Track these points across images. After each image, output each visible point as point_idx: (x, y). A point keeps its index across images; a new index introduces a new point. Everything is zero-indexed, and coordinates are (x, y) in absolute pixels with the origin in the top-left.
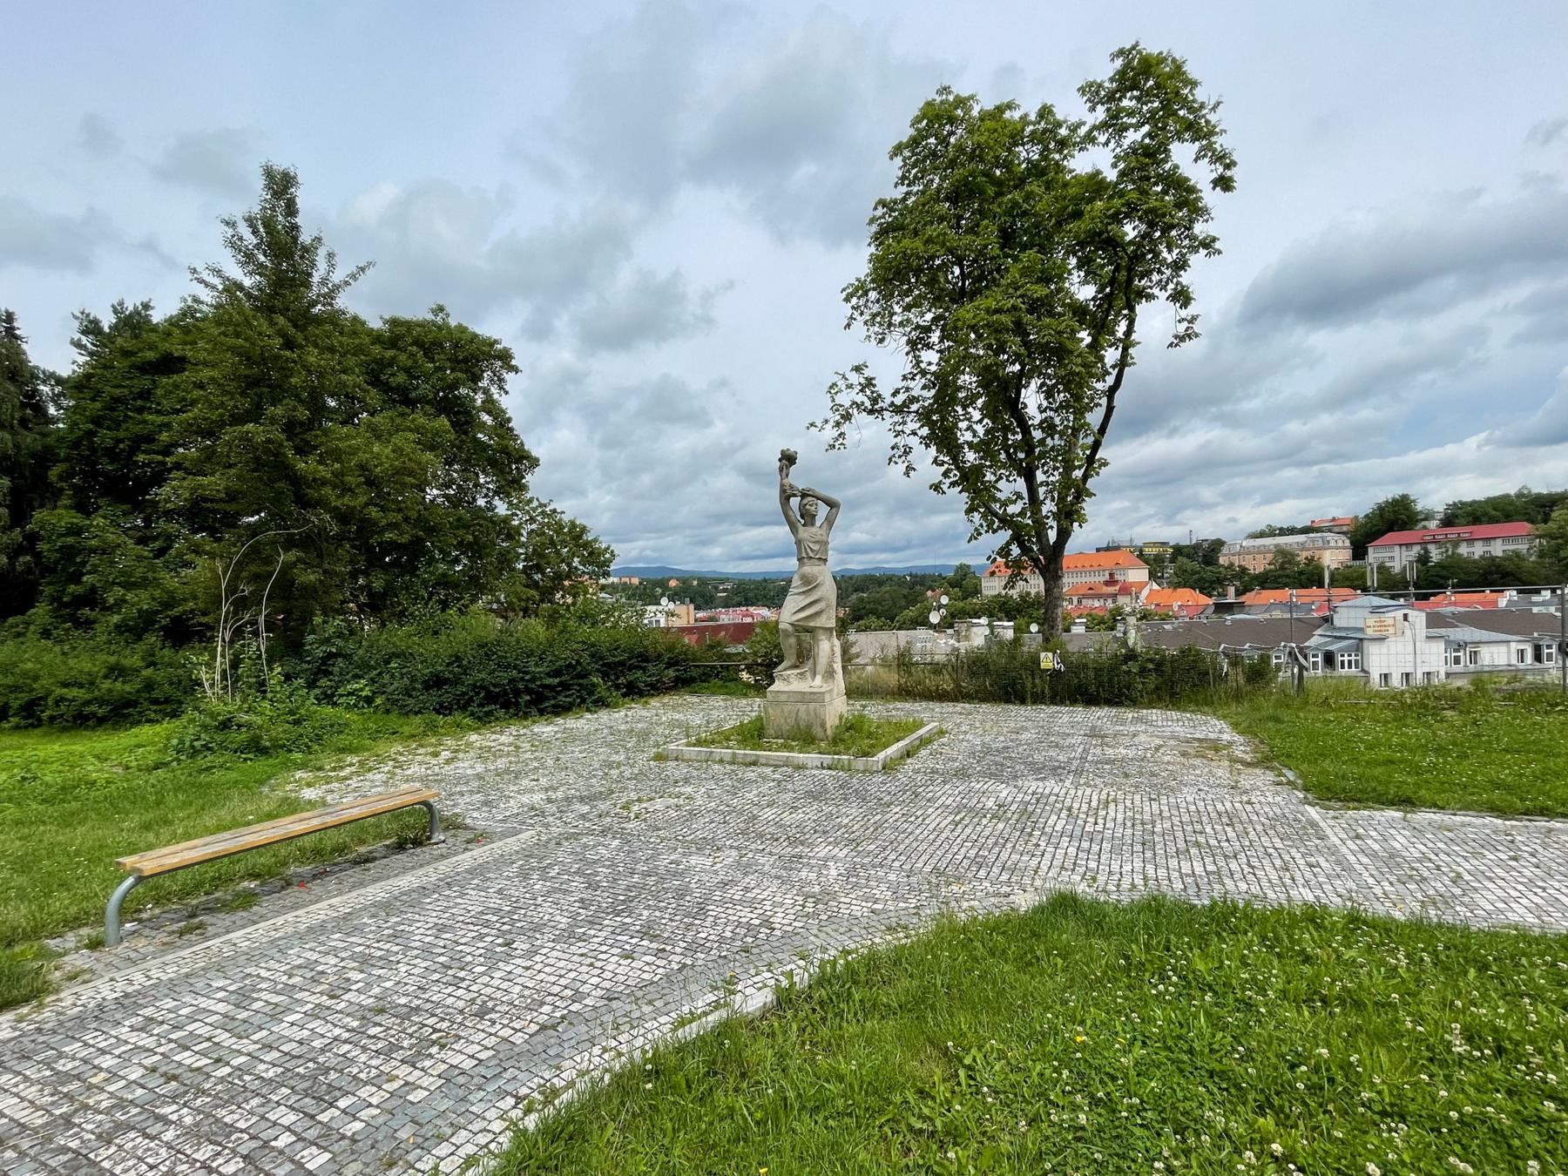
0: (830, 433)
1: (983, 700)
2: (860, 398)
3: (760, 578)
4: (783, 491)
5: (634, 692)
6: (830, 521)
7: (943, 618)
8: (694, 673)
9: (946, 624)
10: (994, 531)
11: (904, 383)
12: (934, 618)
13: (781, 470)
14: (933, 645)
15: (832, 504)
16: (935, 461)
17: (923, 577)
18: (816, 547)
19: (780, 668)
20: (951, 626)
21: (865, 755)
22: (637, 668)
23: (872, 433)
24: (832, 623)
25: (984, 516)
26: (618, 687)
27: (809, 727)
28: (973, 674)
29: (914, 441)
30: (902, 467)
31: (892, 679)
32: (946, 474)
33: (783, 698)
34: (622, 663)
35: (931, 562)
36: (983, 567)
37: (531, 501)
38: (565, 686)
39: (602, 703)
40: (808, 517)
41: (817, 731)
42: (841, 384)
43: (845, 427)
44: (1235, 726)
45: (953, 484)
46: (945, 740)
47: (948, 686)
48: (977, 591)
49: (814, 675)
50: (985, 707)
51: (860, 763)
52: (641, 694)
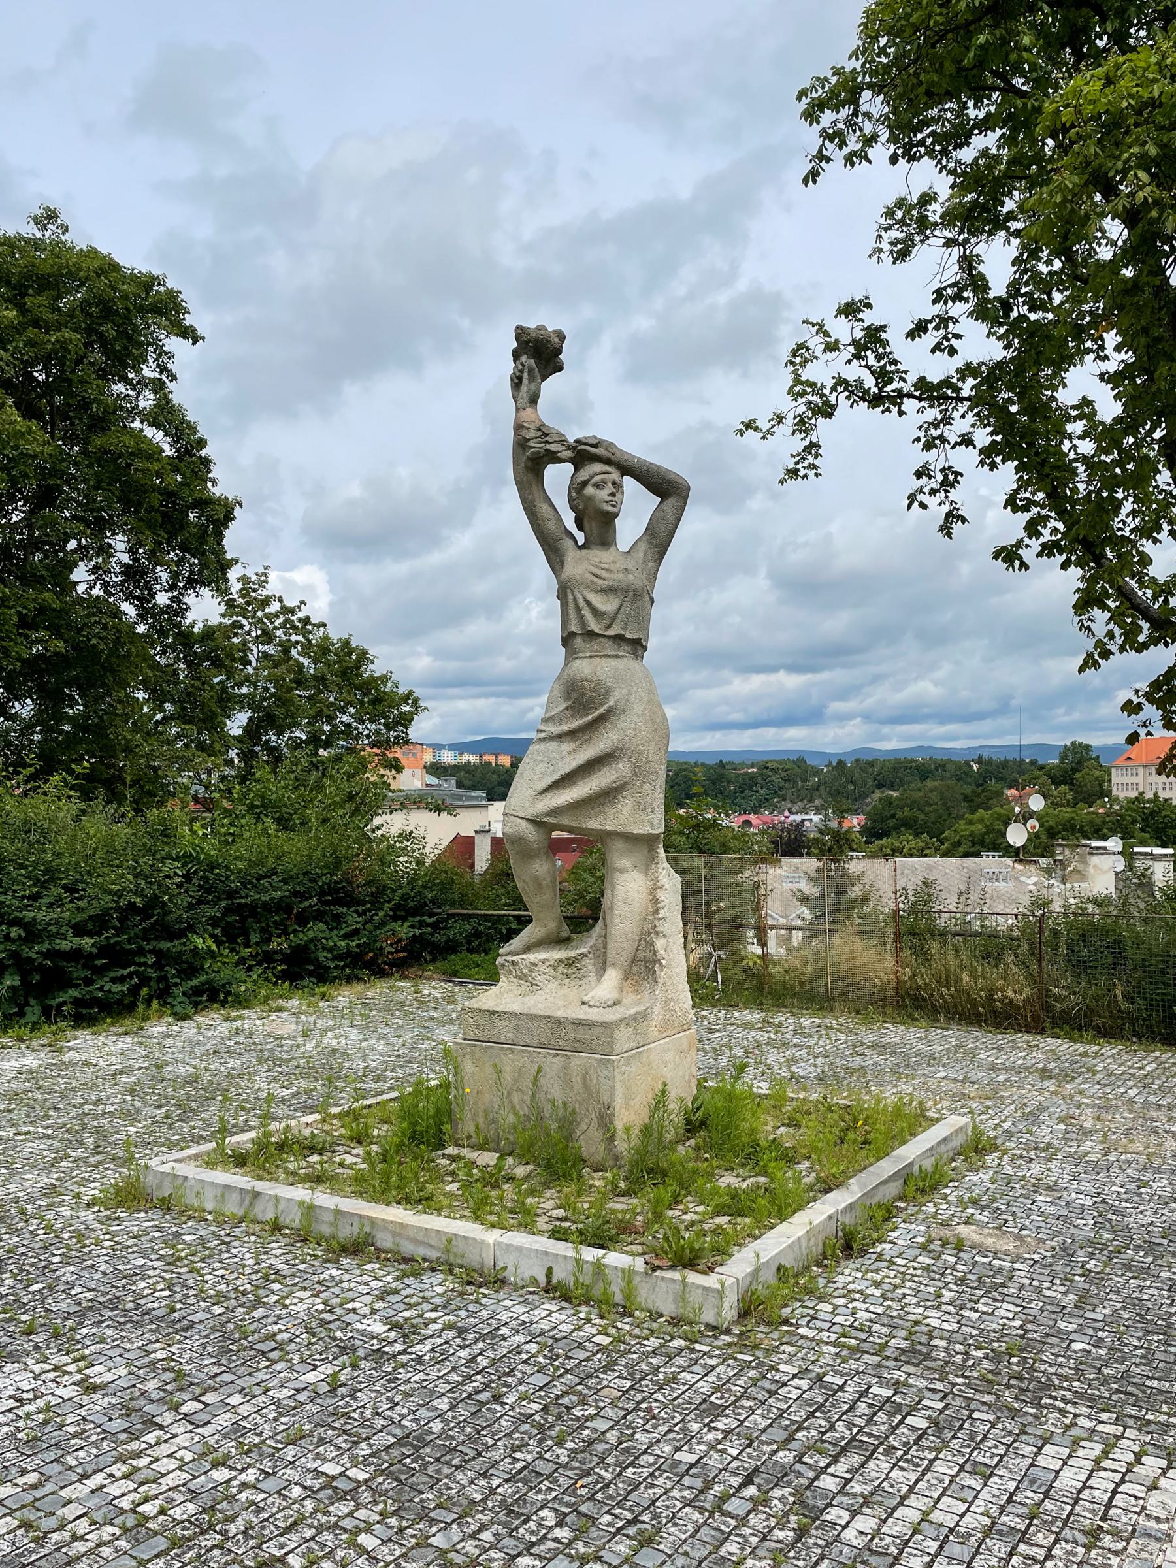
1: (1108, 1034)
2: (854, 372)
3: (712, 762)
4: (521, 444)
5: (303, 971)
6: (659, 538)
7: (1033, 838)
8: (457, 931)
9: (1038, 849)
10: (1144, 647)
11: (937, 309)
12: (1016, 836)
13: (517, 382)
14: (1000, 890)
15: (666, 488)
16: (1012, 503)
17: (1004, 764)
18: (608, 605)
19: (516, 943)
20: (1047, 851)
21: (688, 1260)
22: (319, 916)
23: (874, 447)
24: (654, 822)
25: (1116, 617)
26: (268, 958)
27: (568, 1125)
28: (1080, 966)
29: (965, 459)
30: (937, 510)
31: (880, 964)
32: (1032, 529)
33: (505, 1031)
34: (283, 907)
35: (1012, 740)
36: (1114, 750)
37: (266, 601)
38: (115, 956)
39: (214, 996)
40: (598, 523)
41: (589, 1142)
42: (816, 343)
43: (823, 428)
44: (331, 583)
45: (1048, 549)
46: (980, 1179)
47: (1015, 989)
48: (1101, 790)
50: (1110, 1056)
51: (663, 1291)
52: (323, 976)
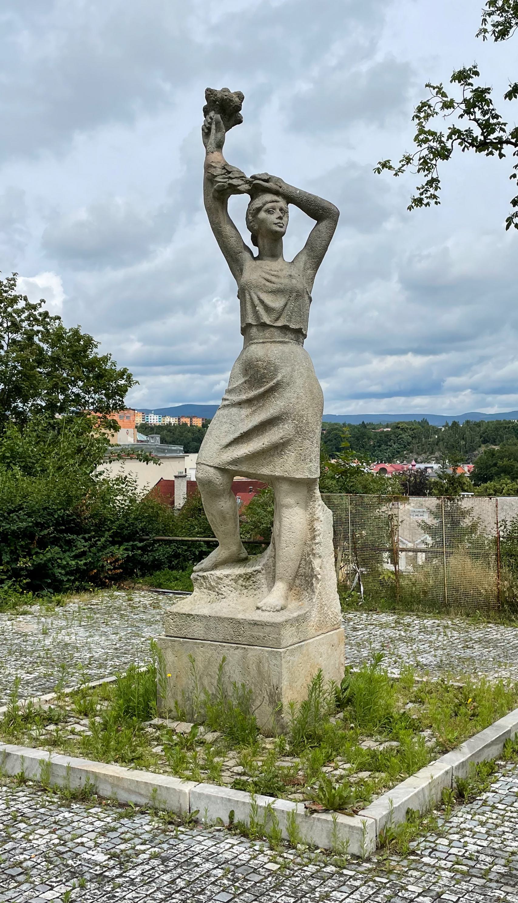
0: (414, 179)
2: (465, 124)
4: (210, 179)
6: (316, 251)
8: (161, 553)
15: (321, 213)
18: (276, 303)
19: (206, 562)
22: (55, 542)
24: (312, 469)
26: (16, 574)
27: (246, 702)
33: (198, 629)
34: (27, 534)
37: (15, 300)
40: (269, 241)
41: (263, 715)
42: (436, 102)
43: (441, 167)
49: (273, 580)
51: (319, 829)
52: (58, 588)
